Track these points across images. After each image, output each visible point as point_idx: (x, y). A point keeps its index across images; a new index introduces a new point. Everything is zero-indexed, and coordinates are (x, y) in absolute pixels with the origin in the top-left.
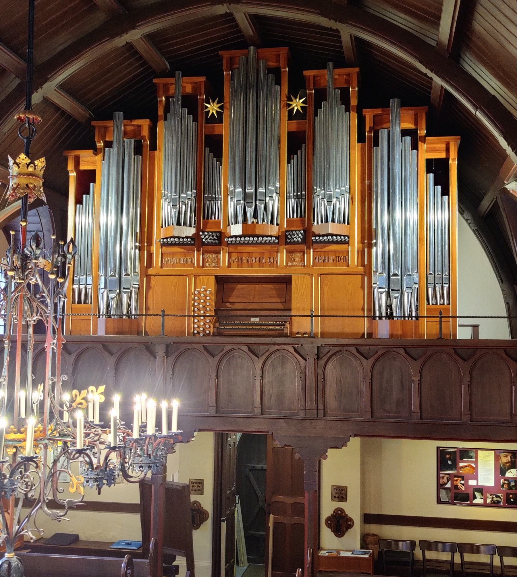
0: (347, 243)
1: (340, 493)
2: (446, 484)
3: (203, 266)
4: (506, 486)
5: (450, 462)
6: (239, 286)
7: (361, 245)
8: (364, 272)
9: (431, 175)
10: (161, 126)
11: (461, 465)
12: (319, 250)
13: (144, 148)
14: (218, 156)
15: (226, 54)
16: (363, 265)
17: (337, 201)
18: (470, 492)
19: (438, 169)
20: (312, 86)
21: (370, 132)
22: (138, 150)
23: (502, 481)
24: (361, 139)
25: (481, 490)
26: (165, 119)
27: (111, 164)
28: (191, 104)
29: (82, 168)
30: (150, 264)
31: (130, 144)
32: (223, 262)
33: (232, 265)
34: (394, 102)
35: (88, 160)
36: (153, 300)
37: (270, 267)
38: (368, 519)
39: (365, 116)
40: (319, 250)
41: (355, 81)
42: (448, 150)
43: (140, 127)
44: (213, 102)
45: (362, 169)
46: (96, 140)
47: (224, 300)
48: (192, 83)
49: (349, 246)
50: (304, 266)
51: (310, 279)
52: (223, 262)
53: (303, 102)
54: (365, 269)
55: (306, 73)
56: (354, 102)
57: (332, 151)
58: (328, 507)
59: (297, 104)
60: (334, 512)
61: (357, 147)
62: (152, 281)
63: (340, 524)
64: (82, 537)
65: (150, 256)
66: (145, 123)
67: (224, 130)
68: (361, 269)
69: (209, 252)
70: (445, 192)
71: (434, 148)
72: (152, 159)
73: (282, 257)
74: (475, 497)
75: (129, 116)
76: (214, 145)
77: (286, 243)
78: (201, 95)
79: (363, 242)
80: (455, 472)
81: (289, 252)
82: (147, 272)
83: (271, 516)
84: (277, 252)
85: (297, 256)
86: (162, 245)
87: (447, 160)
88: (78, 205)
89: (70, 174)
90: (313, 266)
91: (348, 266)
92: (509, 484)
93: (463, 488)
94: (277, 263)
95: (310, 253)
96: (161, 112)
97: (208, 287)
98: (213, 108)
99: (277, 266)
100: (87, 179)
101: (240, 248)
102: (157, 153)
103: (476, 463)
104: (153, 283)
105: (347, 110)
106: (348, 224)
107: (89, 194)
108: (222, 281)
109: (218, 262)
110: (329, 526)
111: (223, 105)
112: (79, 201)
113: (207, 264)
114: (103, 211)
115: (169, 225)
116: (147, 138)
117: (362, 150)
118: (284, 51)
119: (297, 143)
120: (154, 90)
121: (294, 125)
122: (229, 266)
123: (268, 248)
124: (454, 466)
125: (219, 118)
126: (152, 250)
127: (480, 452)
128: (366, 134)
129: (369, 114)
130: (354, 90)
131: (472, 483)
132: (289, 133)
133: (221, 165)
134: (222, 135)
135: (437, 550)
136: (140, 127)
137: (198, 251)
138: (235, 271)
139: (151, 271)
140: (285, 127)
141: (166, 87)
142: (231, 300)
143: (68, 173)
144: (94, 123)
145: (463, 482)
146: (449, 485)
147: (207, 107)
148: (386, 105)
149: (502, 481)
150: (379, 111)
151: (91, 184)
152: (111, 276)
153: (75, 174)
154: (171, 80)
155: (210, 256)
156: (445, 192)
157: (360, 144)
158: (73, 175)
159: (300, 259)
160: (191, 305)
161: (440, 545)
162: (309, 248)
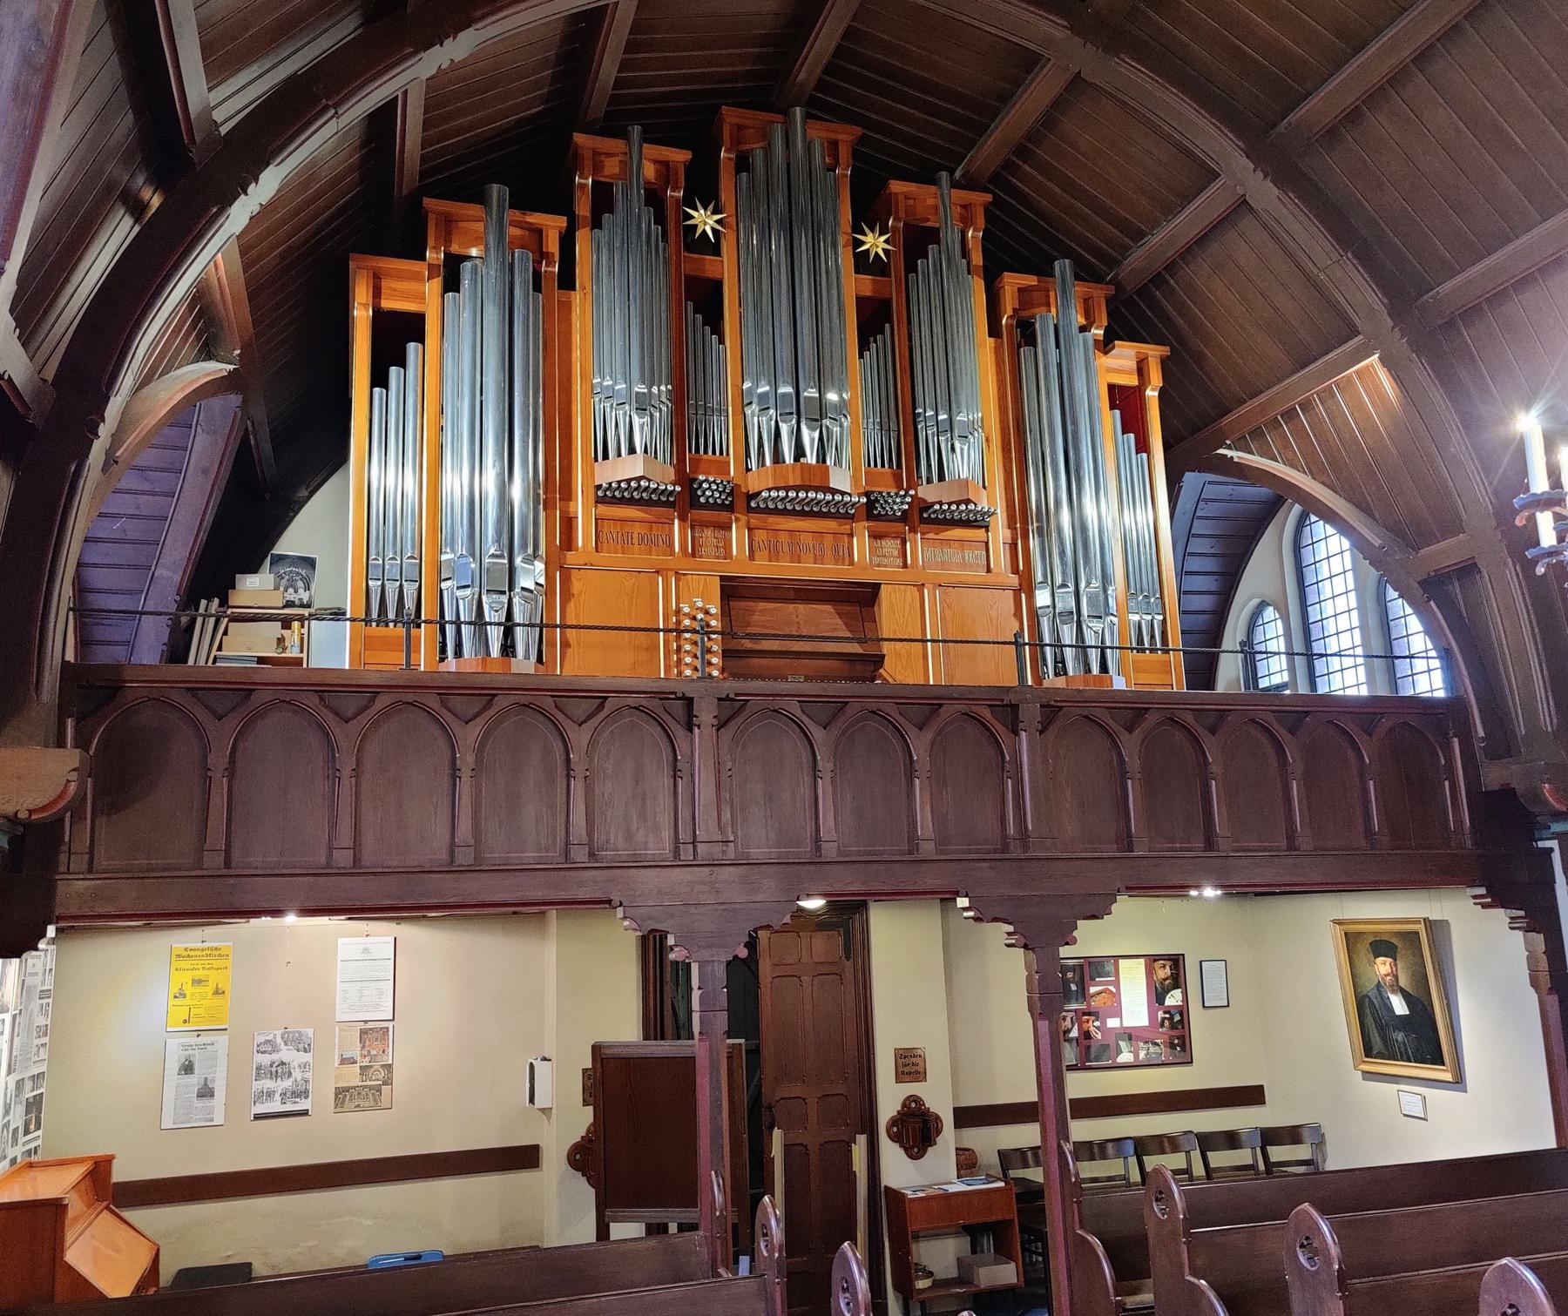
1: (910, 1066)
2: (1069, 1031)
3: (693, 555)
4: (1167, 1023)
5: (1074, 987)
6: (762, 605)
7: (1008, 532)
9: (1117, 412)
11: (1093, 990)
12: (931, 536)
14: (714, 321)
15: (731, 116)
16: (1015, 570)
18: (1111, 1041)
19: (1125, 401)
21: (1011, 317)
23: (1160, 1014)
24: (994, 331)
25: (1130, 1035)
29: (387, 304)
30: (568, 542)
34: (1062, 266)
35: (411, 288)
48: (655, 162)
50: (905, 566)
55: (897, 187)
56: (977, 259)
58: (890, 1099)
59: (875, 243)
60: (904, 1105)
63: (917, 1130)
64: (260, 1269)
65: (569, 523)
66: (552, 225)
67: (726, 268)
68: (1014, 580)
69: (704, 525)
71: (1121, 363)
72: (566, 307)
73: (861, 545)
74: (1119, 1051)
75: (521, 202)
76: (704, 300)
79: (1011, 525)
80: (1083, 1007)
81: (875, 536)
82: (562, 559)
83: (777, 1134)
84: (851, 535)
85: (891, 546)
87: (1139, 391)
88: (377, 390)
91: (989, 570)
92: (1171, 1019)
93: (1099, 1036)
96: (583, 208)
97: (705, 602)
98: (704, 220)
99: (852, 563)
100: (397, 335)
102: (576, 297)
103: (1117, 984)
104: (576, 586)
110: (895, 1138)
112: (379, 379)
117: (998, 350)
119: (874, 319)
120: (569, 162)
121: (866, 284)
122: (752, 557)
124: (1083, 993)
127: (1122, 962)
129: (1012, 283)
131: (1113, 1023)
132: (858, 299)
133: (721, 341)
135: (1104, 1157)
137: (682, 519)
138: (763, 568)
139: (570, 557)
140: (853, 285)
144: (428, 202)
145: (1097, 1024)
146: (1074, 1033)
148: (1045, 271)
149: (1160, 1014)
150: (1031, 280)
152: (493, 556)
154: (616, 145)
155: (708, 533)
156: (1143, 446)
158: (362, 316)
161: (1110, 1148)
162: (913, 530)
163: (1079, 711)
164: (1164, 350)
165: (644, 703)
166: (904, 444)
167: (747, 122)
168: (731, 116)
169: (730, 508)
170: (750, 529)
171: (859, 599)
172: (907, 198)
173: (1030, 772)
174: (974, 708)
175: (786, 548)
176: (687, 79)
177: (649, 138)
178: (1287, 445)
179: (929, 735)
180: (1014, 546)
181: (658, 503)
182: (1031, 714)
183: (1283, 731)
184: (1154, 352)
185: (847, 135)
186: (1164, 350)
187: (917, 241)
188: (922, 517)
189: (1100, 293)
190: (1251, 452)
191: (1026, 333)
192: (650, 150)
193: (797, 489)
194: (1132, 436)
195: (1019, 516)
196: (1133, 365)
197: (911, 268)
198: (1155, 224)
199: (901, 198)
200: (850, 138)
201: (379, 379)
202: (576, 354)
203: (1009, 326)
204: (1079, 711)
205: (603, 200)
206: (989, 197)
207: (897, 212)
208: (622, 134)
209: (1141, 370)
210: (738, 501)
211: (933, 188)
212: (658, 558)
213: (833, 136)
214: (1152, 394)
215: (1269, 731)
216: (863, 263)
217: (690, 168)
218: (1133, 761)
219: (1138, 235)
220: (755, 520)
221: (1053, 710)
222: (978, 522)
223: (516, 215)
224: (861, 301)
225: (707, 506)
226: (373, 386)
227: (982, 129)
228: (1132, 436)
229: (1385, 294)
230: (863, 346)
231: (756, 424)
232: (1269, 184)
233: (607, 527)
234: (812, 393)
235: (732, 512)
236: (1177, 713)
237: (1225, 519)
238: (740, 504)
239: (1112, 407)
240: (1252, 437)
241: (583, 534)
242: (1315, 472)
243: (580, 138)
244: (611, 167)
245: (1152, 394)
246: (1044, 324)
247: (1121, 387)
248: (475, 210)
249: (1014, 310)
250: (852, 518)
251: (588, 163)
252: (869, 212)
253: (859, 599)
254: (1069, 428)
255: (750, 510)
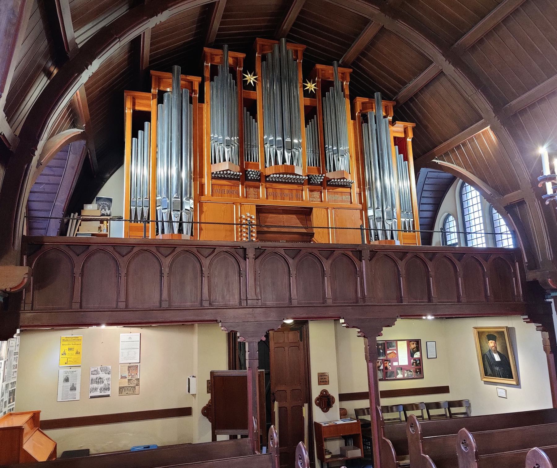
1: (323, 379)
2: (380, 367)
3: (246, 197)
4: (414, 364)
5: (381, 351)
6: (271, 215)
7: (358, 189)
9: (397, 147)
11: (388, 352)
12: (331, 190)
14: (254, 114)
15: (260, 41)
16: (361, 203)
18: (395, 370)
19: (400, 143)
21: (359, 113)
23: (412, 361)
24: (353, 118)
25: (402, 368)
29: (137, 108)
30: (202, 193)
34: (377, 95)
35: (146, 102)
38: (343, 397)
48: (233, 58)
50: (322, 201)
55: (319, 66)
56: (347, 92)
58: (316, 391)
59: (311, 86)
60: (321, 393)
63: (326, 402)
64: (92, 451)
65: (202, 186)
66: (196, 80)
67: (258, 95)
68: (360, 206)
69: (250, 187)
71: (398, 129)
72: (201, 109)
73: (306, 194)
74: (398, 374)
75: (185, 72)
76: (250, 107)
79: (359, 187)
80: (385, 358)
81: (311, 191)
82: (200, 199)
83: (276, 403)
84: (302, 190)
85: (316, 194)
87: (405, 139)
88: (134, 139)
91: (351, 203)
92: (416, 362)
93: (390, 369)
96: (207, 74)
97: (250, 214)
98: (250, 78)
99: (302, 200)
100: (141, 119)
102: (205, 106)
103: (397, 350)
104: (205, 208)
110: (318, 405)
111: (304, 88)
112: (135, 135)
117: (354, 125)
119: (310, 113)
120: (202, 58)
121: (308, 101)
122: (267, 198)
124: (385, 353)
127: (398, 342)
129: (359, 101)
131: (395, 364)
132: (305, 106)
133: (256, 121)
135: (392, 411)
137: (242, 185)
138: (271, 202)
139: (203, 198)
140: (303, 101)
144: (152, 72)
145: (390, 364)
146: (382, 368)
148: (371, 96)
149: (412, 361)
150: (366, 100)
152: (175, 198)
154: (219, 52)
155: (252, 189)
156: (406, 159)
158: (128, 113)
161: (394, 408)
162: (324, 189)
163: (383, 253)
164: (414, 125)
165: (229, 250)
166: (321, 158)
167: (265, 44)
168: (260, 41)
169: (259, 181)
170: (266, 188)
171: (305, 213)
172: (322, 70)
173: (366, 274)
174: (346, 252)
175: (279, 195)
176: (244, 28)
177: (231, 49)
178: (457, 158)
179: (330, 261)
180: (360, 194)
181: (234, 179)
182: (366, 254)
183: (456, 260)
184: (410, 125)
185: (301, 48)
186: (414, 125)
187: (326, 86)
188: (328, 184)
189: (391, 104)
190: (444, 161)
191: (365, 118)
192: (231, 53)
193: (283, 174)
194: (402, 155)
195: (362, 184)
196: (403, 130)
197: (324, 95)
198: (410, 80)
199: (320, 70)
200: (302, 49)
201: (135, 135)
202: (205, 126)
203: (358, 116)
204: (383, 253)
205: (214, 71)
206: (351, 70)
207: (319, 75)
208: (221, 48)
209: (405, 132)
210: (262, 178)
211: (331, 67)
212: (234, 199)
213: (296, 48)
214: (409, 140)
215: (451, 260)
216: (306, 93)
217: (245, 60)
218: (402, 271)
219: (404, 84)
220: (268, 185)
221: (374, 252)
222: (347, 186)
223: (183, 76)
224: (306, 107)
225: (251, 180)
226: (132, 137)
227: (349, 46)
228: (402, 155)
229: (492, 105)
230: (307, 123)
231: (269, 151)
232: (451, 65)
233: (216, 187)
234: (288, 140)
235: (260, 182)
236: (418, 253)
237: (435, 184)
238: (263, 179)
239: (395, 145)
240: (445, 156)
241: (207, 190)
242: (467, 168)
243: (206, 49)
244: (217, 60)
245: (409, 140)
246: (371, 115)
247: (398, 138)
248: (169, 75)
249: (360, 110)
250: (303, 184)
251: (209, 58)
252: (309, 75)
253: (305, 213)
254: (380, 152)
255: (266, 181)
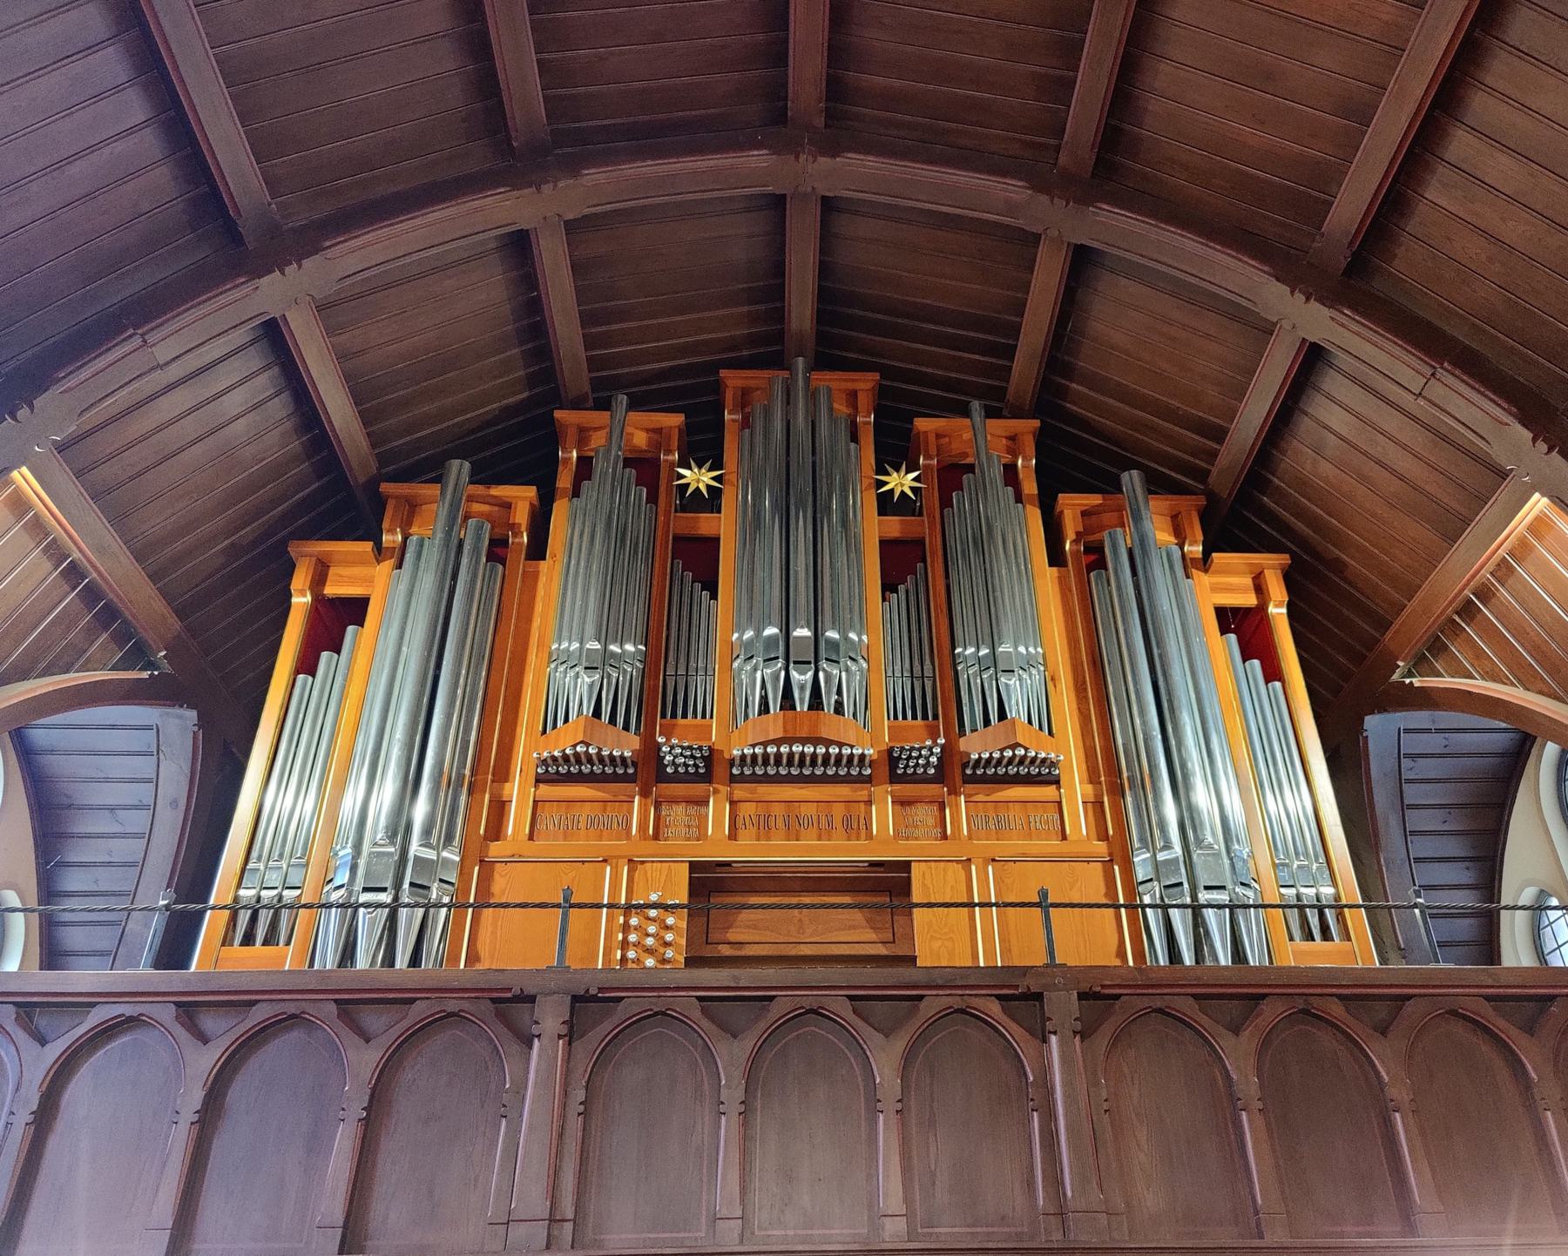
0: (1056, 782)
3: (656, 837)
7: (1089, 788)
8: (1110, 854)
9: (1233, 637)
10: (561, 510)
12: (980, 797)
13: (513, 553)
15: (733, 380)
16: (1103, 836)
17: (1026, 669)
19: (1243, 626)
20: (933, 451)
21: (1074, 542)
22: (497, 550)
24: (1056, 557)
26: (576, 493)
27: (422, 565)
28: (645, 468)
29: (330, 590)
30: (496, 830)
31: (475, 536)
32: (715, 828)
33: (741, 832)
34: (1132, 480)
35: (351, 570)
36: (494, 933)
37: (849, 839)
39: (1062, 512)
40: (980, 797)
41: (1030, 446)
42: (1259, 588)
43: (507, 506)
44: (700, 467)
45: (1066, 622)
46: (385, 525)
47: (713, 937)
48: (647, 430)
49: (1059, 788)
50: (945, 837)
51: (962, 874)
52: (715, 828)
53: (914, 480)
54: (1109, 847)
55: (921, 424)
56: (1030, 487)
57: (1002, 571)
59: (901, 482)
61: (1047, 578)
62: (496, 876)
65: (499, 808)
66: (523, 496)
67: (725, 525)
68: (1101, 847)
69: (674, 801)
70: (1273, 672)
71: (1232, 580)
72: (531, 579)
73: (883, 814)
75: (485, 474)
76: (699, 560)
77: (894, 779)
78: (669, 452)
79: (1093, 778)
82: (484, 850)
84: (869, 803)
85: (924, 815)
86: (539, 780)
87: (1261, 608)
89: (294, 600)
90: (970, 837)
91: (1064, 837)
94: (868, 827)
95: (958, 805)
96: (564, 480)
98: (698, 478)
99: (869, 836)
100: (337, 619)
101: (765, 790)
105: (1019, 498)
106: (1050, 733)
107: (338, 653)
108: (711, 885)
109: (702, 826)
112: (307, 665)
113: (664, 832)
114: (356, 787)
115: (566, 720)
116: (523, 528)
118: (865, 383)
119: (900, 562)
120: (552, 437)
121: (894, 526)
122: (733, 836)
123: (843, 791)
125: (711, 501)
126: (506, 792)
128: (1067, 547)
129: (1071, 506)
130: (1026, 465)
133: (714, 596)
134: (718, 539)
136: (507, 506)
137: (645, 794)
138: (748, 851)
139: (496, 850)
140: (873, 528)
141: (583, 435)
142: (732, 936)
143: (288, 596)
144: (386, 487)
147: (681, 477)
150: (1095, 500)
151: (351, 629)
153: (309, 598)
154: (600, 417)
155: (679, 809)
156: (1273, 672)
157: (1055, 569)
158: (301, 600)
159: (931, 821)
160: (614, 944)
162: (954, 792)
163: (1146, 1002)
164: (1284, 559)
165: (466, 1005)
166: (937, 695)
167: (752, 383)
168: (733, 380)
169: (707, 778)
170: (732, 803)
171: (887, 886)
172: (938, 436)
173: (1066, 1095)
174: (976, 1002)
175: (780, 822)
176: (685, 350)
177: (635, 404)
178: (1479, 654)
179: (899, 1044)
180: (1098, 804)
181: (615, 778)
182: (1063, 1006)
183: (1514, 1031)
184: (1272, 565)
185: (865, 383)
186: (1284, 559)
187: (952, 475)
188: (955, 773)
189: (1190, 506)
190: (1439, 675)
191: (1095, 557)
192: (635, 417)
193: (778, 742)
194: (1256, 663)
195: (1113, 777)
196: (1248, 581)
197: (946, 502)
198: (1231, 414)
199: (932, 438)
200: (869, 385)
201: (307, 665)
202: (536, 623)
203: (1075, 553)
204: (1146, 1002)
205: (585, 468)
206: (1036, 423)
207: (927, 451)
208: (604, 405)
209: (1259, 588)
210: (708, 767)
211: (967, 421)
212: (608, 844)
213: (850, 386)
214: (1278, 612)
215: (1486, 1030)
216: (887, 504)
217: (688, 430)
218: (1248, 1083)
219: (1219, 434)
220: (740, 791)
221: (1099, 997)
222: (1045, 775)
223: (479, 490)
224: (885, 544)
225: (676, 778)
226: (297, 672)
227: (1009, 352)
228: (1256, 663)
229: (1509, 400)
230: (888, 587)
231: (740, 675)
232: (1314, 306)
233: (546, 813)
234: (802, 632)
235: (710, 782)
236: (1315, 1001)
237: (1462, 780)
238: (720, 771)
239: (1223, 632)
240: (1433, 650)
241: (516, 821)
242: (1527, 679)
243: (558, 414)
244: (598, 440)
245: (1278, 612)
246: (1120, 542)
247: (1236, 611)
248: (433, 490)
249: (1078, 534)
250: (869, 780)
251: (571, 436)
252: (895, 451)
253: (887, 886)
254: (1155, 651)
255: (733, 779)
